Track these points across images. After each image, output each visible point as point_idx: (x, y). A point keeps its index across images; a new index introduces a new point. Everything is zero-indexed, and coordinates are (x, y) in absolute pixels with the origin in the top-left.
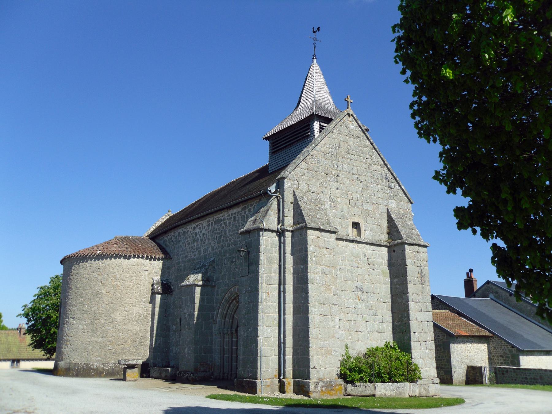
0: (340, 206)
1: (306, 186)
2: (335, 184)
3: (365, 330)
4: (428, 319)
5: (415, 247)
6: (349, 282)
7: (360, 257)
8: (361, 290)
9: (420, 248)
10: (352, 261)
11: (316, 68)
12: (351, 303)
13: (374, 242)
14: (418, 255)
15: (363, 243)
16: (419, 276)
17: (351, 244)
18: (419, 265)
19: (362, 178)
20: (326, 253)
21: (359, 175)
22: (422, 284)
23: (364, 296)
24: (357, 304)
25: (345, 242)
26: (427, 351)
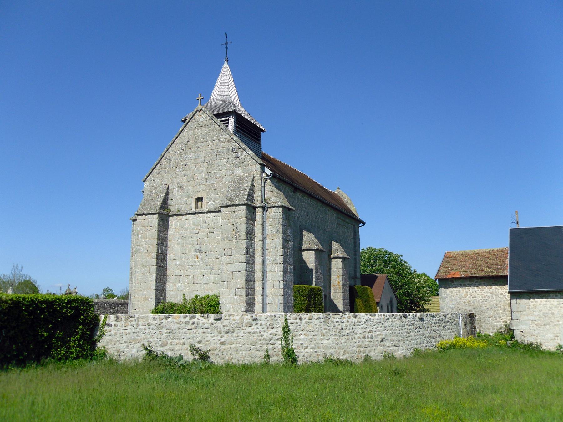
0: (186, 189)
1: (159, 181)
2: (183, 173)
3: (201, 282)
4: (239, 269)
5: (231, 207)
6: (189, 246)
7: (200, 225)
8: (200, 250)
9: (237, 207)
10: (193, 229)
11: (226, 68)
12: (191, 262)
13: (212, 210)
14: (235, 214)
15: (204, 213)
16: (234, 233)
17: (193, 216)
18: (234, 223)
19: (208, 159)
20: (149, 229)
21: (205, 157)
22: (236, 239)
23: (202, 256)
24: (195, 262)
25: (187, 216)
26: (236, 297)
